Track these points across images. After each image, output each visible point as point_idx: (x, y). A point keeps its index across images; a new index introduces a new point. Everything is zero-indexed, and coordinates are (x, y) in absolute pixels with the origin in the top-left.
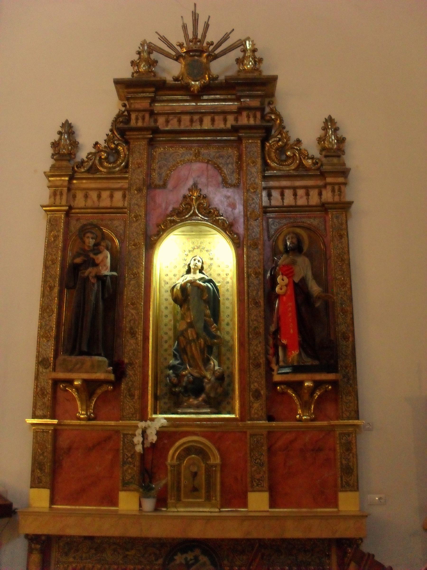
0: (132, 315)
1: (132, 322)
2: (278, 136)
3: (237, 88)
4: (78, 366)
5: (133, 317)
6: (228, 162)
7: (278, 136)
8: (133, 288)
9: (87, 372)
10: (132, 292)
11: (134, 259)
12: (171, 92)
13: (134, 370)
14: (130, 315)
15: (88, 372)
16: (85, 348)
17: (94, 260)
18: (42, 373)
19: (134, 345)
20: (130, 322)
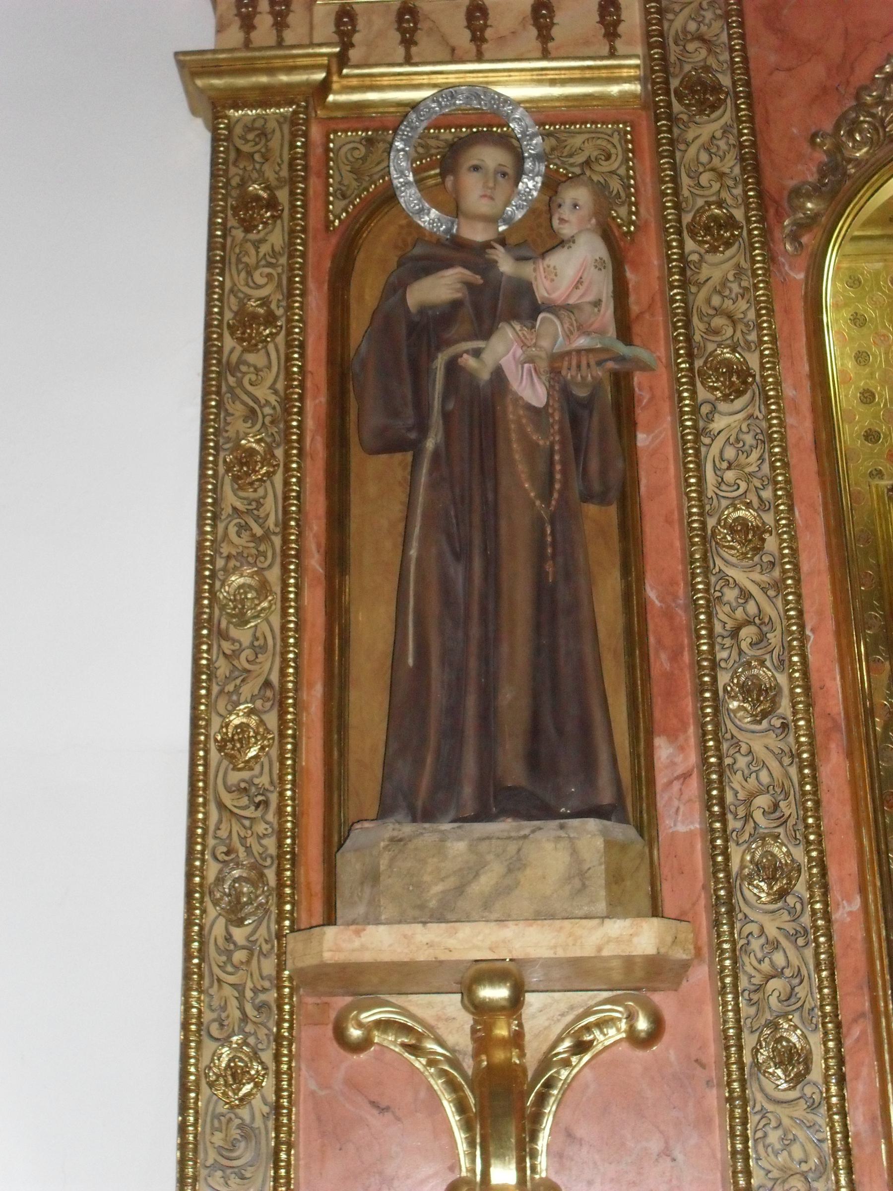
0: (746, 595)
1: (748, 633)
2: (337, 221)
3: (383, 488)
4: (486, 882)
5: (751, 608)
6: (708, 135)
7: (337, 221)
8: (730, 453)
9: (543, 914)
10: (730, 476)
11: (716, 301)
12: (599, 733)
13: (791, 911)
14: (730, 595)
15: (552, 917)
16: (513, 769)
17: (524, 289)
18: (229, 954)
19: (773, 764)
20: (735, 633)
